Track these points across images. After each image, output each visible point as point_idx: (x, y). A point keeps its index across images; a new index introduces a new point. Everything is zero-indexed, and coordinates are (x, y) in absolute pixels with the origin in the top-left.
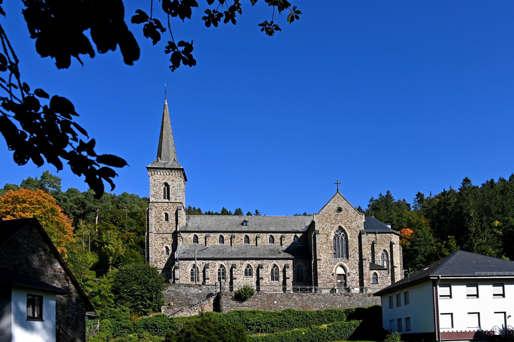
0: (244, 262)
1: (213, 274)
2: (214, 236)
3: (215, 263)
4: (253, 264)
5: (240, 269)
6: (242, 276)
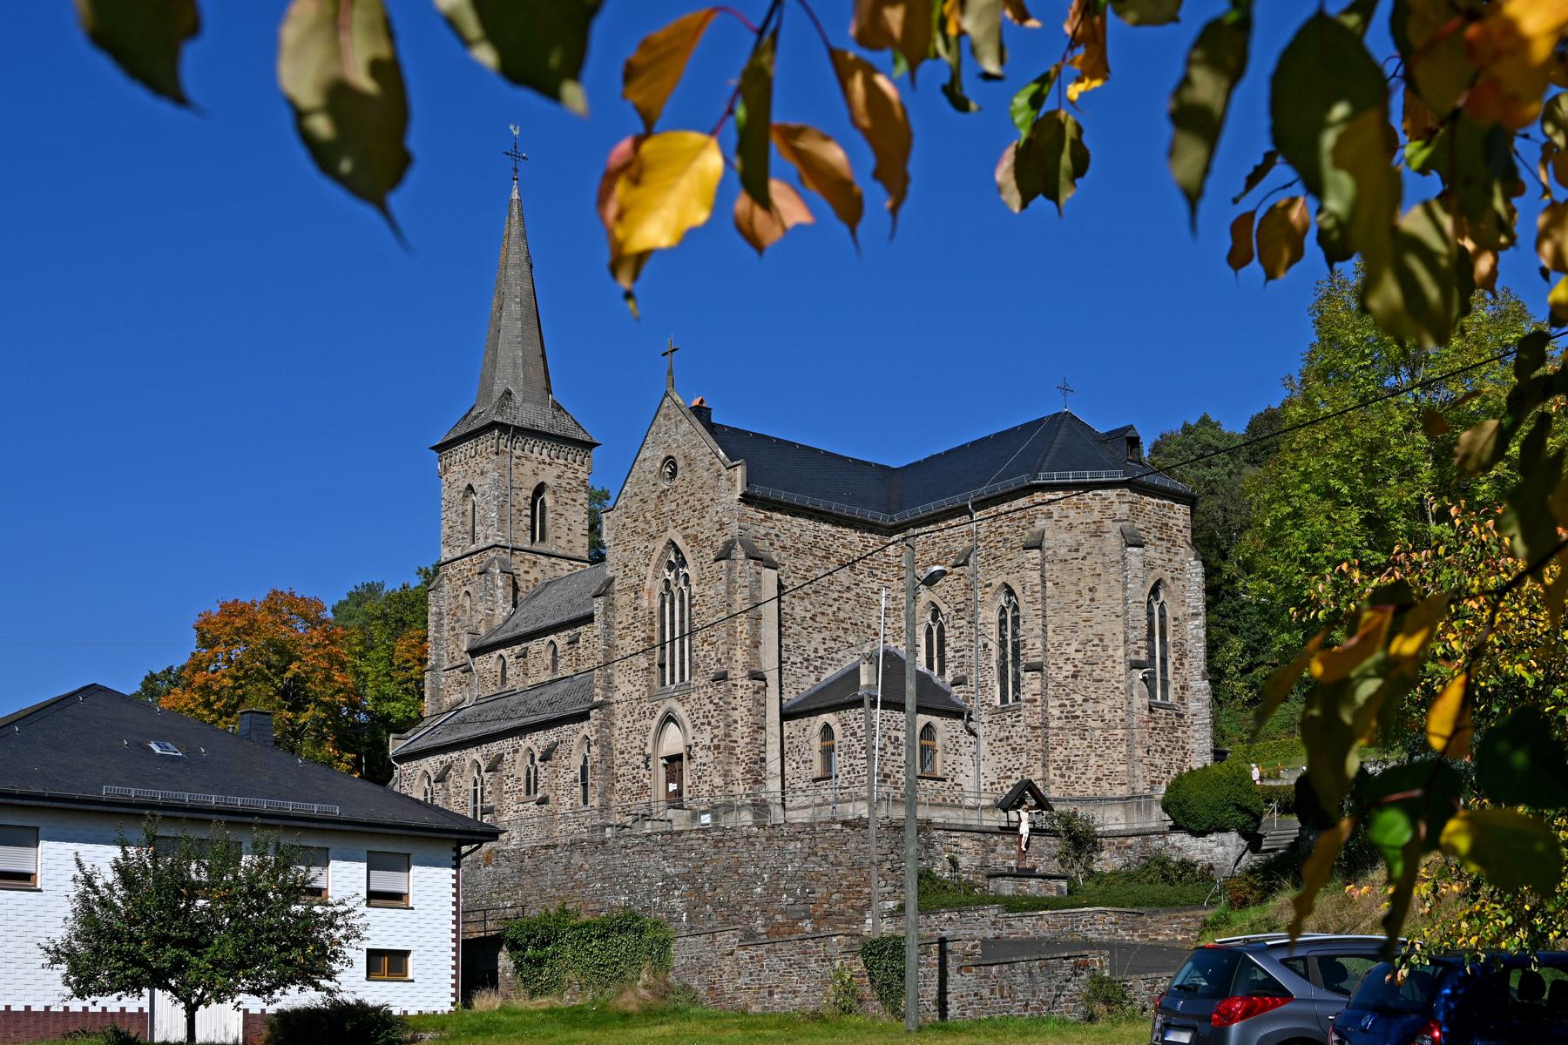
0: (521, 742)
2: (537, 648)
5: (513, 770)
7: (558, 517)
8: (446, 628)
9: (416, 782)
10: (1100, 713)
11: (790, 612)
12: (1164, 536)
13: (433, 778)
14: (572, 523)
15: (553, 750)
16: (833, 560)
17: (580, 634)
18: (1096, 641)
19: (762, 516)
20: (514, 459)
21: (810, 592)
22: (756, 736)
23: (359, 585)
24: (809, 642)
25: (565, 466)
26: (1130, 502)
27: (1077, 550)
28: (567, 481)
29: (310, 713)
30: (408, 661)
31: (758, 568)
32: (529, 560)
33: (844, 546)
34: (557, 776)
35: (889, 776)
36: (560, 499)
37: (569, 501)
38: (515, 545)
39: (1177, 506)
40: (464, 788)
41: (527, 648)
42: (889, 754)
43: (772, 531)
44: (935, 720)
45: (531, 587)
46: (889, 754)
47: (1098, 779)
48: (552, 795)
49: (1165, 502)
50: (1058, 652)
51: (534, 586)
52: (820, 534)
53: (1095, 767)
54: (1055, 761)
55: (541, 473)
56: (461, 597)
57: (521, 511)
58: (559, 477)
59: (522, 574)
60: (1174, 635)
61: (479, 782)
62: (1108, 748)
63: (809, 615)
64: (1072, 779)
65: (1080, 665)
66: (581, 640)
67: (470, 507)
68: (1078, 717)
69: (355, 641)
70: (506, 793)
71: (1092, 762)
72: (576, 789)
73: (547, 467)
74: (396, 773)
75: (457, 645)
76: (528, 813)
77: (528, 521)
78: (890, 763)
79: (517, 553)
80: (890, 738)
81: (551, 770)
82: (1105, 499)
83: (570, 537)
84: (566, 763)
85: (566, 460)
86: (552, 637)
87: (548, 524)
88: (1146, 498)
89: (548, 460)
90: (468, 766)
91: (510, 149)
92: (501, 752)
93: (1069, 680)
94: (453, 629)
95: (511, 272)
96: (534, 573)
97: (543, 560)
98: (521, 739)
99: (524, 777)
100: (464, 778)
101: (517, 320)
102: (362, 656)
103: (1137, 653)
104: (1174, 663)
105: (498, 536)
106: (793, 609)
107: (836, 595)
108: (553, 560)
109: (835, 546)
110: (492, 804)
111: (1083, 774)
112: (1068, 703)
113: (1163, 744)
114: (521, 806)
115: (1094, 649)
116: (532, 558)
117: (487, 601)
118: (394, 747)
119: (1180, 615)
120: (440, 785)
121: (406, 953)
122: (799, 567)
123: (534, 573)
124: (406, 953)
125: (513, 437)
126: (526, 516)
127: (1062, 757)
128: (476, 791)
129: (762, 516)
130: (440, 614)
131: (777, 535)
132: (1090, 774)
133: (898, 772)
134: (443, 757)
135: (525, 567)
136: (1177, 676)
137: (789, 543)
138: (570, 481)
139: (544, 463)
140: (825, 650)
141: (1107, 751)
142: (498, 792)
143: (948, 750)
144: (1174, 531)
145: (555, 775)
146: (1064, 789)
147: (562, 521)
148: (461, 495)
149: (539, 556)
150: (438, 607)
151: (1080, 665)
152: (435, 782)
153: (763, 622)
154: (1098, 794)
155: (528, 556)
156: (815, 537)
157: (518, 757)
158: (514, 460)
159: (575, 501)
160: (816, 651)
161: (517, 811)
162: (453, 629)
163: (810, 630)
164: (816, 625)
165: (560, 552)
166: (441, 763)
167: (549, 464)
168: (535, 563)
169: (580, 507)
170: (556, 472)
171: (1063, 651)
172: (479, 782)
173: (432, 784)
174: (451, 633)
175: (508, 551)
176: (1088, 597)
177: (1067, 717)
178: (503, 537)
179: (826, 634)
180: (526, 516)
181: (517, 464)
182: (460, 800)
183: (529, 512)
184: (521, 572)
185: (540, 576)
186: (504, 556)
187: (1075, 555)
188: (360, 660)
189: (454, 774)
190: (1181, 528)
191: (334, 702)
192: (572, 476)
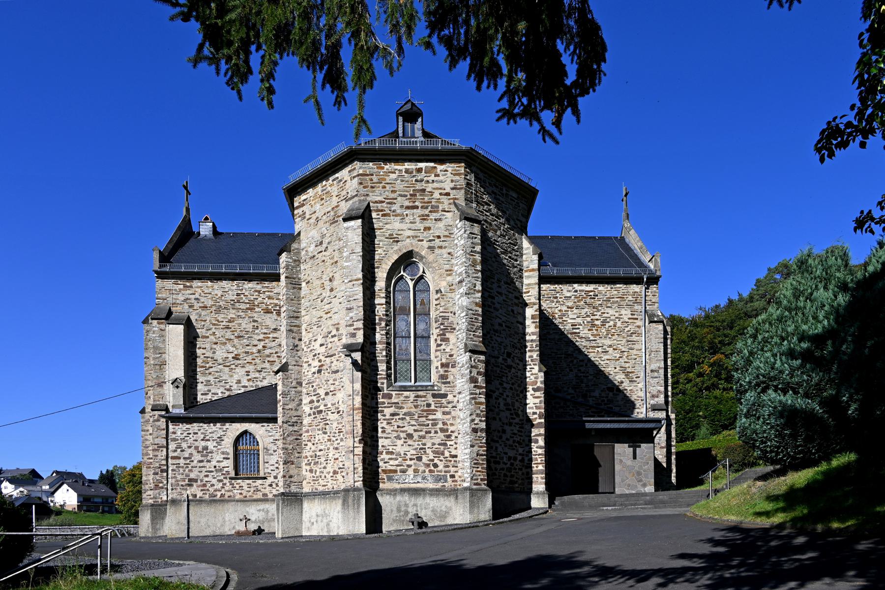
10: (337, 405)
11: (211, 355)
12: (417, 204)
16: (257, 309)
18: (334, 332)
19: (182, 287)
21: (232, 337)
22: (156, 453)
24: (232, 376)
26: (358, 175)
27: (321, 243)
31: (162, 326)
33: (269, 298)
35: (196, 481)
39: (440, 167)
42: (195, 462)
43: (193, 297)
44: (252, 427)
46: (195, 462)
47: (335, 472)
49: (422, 165)
50: (309, 349)
52: (244, 291)
53: (333, 460)
54: (306, 457)
60: (437, 310)
62: (342, 440)
63: (230, 356)
64: (318, 473)
65: (323, 358)
68: (321, 412)
71: (330, 455)
78: (198, 469)
80: (196, 448)
82: (341, 181)
88: (388, 167)
93: (316, 375)
103: (353, 335)
104: (436, 340)
106: (214, 353)
107: (261, 337)
109: (260, 299)
111: (325, 468)
112: (315, 398)
113: (410, 430)
115: (332, 340)
119: (443, 285)
122: (220, 320)
127: (311, 453)
129: (182, 287)
131: (196, 299)
132: (330, 468)
133: (207, 476)
136: (438, 353)
137: (210, 303)
140: (249, 380)
141: (342, 444)
143: (271, 452)
144: (436, 195)
146: (312, 483)
151: (323, 358)
153: (167, 367)
154: (335, 487)
156: (238, 295)
160: (239, 382)
163: (233, 367)
164: (239, 362)
171: (312, 348)
176: (329, 288)
177: (314, 414)
179: (251, 368)
187: (320, 249)
190: (448, 190)
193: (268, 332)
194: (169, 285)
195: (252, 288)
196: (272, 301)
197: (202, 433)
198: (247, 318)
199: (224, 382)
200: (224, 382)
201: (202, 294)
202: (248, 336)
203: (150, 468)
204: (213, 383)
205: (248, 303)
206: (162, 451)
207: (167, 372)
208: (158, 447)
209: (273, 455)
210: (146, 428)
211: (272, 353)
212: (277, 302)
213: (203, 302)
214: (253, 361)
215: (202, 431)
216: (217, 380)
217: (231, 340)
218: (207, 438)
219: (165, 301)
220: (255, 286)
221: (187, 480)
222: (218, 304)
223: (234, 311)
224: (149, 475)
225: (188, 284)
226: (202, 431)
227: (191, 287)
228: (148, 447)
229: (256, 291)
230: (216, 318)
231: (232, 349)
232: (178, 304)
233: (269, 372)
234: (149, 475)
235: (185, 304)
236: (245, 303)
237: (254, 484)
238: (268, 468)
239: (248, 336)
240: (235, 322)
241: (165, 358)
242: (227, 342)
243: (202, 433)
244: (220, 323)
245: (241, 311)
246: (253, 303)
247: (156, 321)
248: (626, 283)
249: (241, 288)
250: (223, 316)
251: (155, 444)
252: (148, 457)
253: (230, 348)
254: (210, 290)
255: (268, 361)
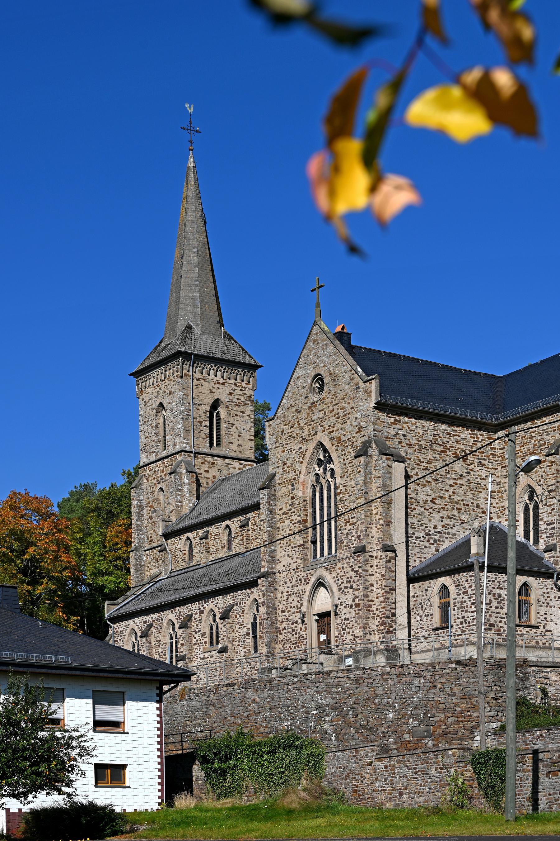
0: (205, 605)
1: (160, 650)
2: (216, 531)
3: (162, 620)
4: (219, 609)
5: (199, 627)
6: (202, 648)
7: (230, 426)
8: (145, 517)
9: (126, 637)
13: (139, 634)
14: (242, 431)
15: (230, 611)
16: (449, 453)
17: (249, 519)
19: (392, 420)
20: (195, 380)
22: (388, 596)
23: (78, 485)
24: (430, 520)
25: (235, 384)
28: (237, 397)
29: (44, 585)
30: (117, 544)
31: (389, 462)
32: (208, 462)
33: (458, 442)
34: (233, 631)
36: (232, 412)
37: (238, 413)
38: (197, 450)
40: (163, 641)
41: (208, 531)
42: (493, 608)
44: (530, 580)
45: (210, 483)
46: (493, 608)
48: (230, 645)
51: (213, 482)
55: (216, 392)
56: (156, 493)
57: (201, 422)
58: (230, 394)
59: (203, 473)
61: (174, 636)
66: (250, 524)
67: (161, 421)
69: (76, 529)
70: (195, 644)
72: (248, 641)
73: (221, 386)
74: (111, 631)
75: (154, 531)
76: (212, 660)
77: (207, 430)
78: (494, 615)
79: (199, 456)
81: (229, 626)
83: (240, 442)
84: (240, 620)
85: (236, 380)
86: (228, 522)
87: (223, 432)
89: (221, 381)
90: (165, 624)
91: (186, 124)
92: (190, 613)
94: (151, 518)
95: (189, 228)
96: (213, 472)
97: (220, 461)
98: (205, 602)
99: (208, 632)
100: (162, 633)
101: (195, 267)
102: (81, 541)
105: (184, 443)
106: (417, 494)
108: (227, 461)
109: (451, 442)
110: (184, 653)
114: (207, 654)
116: (211, 459)
117: (176, 495)
118: (108, 611)
120: (144, 640)
121: (124, 767)
122: (422, 460)
123: (213, 472)
124: (124, 767)
125: (194, 363)
126: (206, 426)
128: (171, 644)
129: (392, 420)
130: (140, 506)
134: (146, 618)
135: (205, 467)
137: (414, 441)
138: (240, 397)
139: (219, 383)
140: (443, 526)
142: (188, 644)
145: (231, 630)
147: (233, 429)
148: (155, 411)
149: (216, 458)
150: (138, 501)
152: (140, 637)
155: (207, 458)
156: (435, 435)
157: (204, 616)
158: (195, 382)
159: (243, 412)
160: (435, 527)
161: (203, 659)
162: (151, 518)
163: (431, 510)
165: (232, 455)
166: (145, 622)
167: (223, 384)
168: (213, 464)
169: (248, 418)
170: (228, 390)
172: (174, 636)
173: (139, 638)
174: (149, 520)
175: (192, 455)
178: (188, 444)
180: (206, 426)
181: (197, 385)
182: (160, 650)
183: (207, 423)
184: (202, 471)
185: (217, 474)
186: (189, 459)
188: (81, 544)
189: (154, 630)
191: (62, 577)
192: (240, 392)
193: (456, 478)
194: (383, 417)
195: (445, 430)
196: (459, 446)
197: (498, 582)
198: (441, 461)
199: (424, 525)
200: (424, 525)
201: (408, 431)
202: (442, 479)
203: (369, 610)
204: (416, 526)
205: (442, 445)
206: (392, 594)
207: (393, 511)
208: (390, 589)
209: (542, 606)
210: (366, 568)
211: (459, 500)
212: (462, 447)
213: (409, 439)
214: (446, 507)
215: (498, 580)
216: (420, 523)
217: (429, 482)
218: (501, 586)
219: (380, 434)
220: (447, 428)
221: (488, 624)
222: (420, 443)
223: (432, 452)
224: (369, 618)
225: (397, 418)
226: (498, 580)
227: (399, 421)
228: (367, 588)
229: (448, 433)
230: (418, 457)
231: (430, 492)
232: (390, 438)
233: (457, 520)
234: (369, 618)
235: (396, 440)
236: (440, 445)
237: (531, 632)
238: (539, 618)
239: (442, 479)
240: (433, 464)
241: (391, 497)
242: (427, 484)
243: (498, 582)
244: (421, 464)
245: (437, 453)
246: (446, 446)
247: (385, 456)
248: (451, 424)
249: (436, 429)
250: (423, 456)
251: (387, 587)
252: (368, 599)
253: (429, 490)
254: (414, 427)
255: (457, 508)
